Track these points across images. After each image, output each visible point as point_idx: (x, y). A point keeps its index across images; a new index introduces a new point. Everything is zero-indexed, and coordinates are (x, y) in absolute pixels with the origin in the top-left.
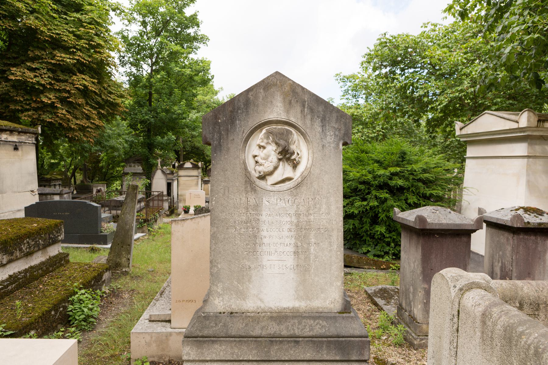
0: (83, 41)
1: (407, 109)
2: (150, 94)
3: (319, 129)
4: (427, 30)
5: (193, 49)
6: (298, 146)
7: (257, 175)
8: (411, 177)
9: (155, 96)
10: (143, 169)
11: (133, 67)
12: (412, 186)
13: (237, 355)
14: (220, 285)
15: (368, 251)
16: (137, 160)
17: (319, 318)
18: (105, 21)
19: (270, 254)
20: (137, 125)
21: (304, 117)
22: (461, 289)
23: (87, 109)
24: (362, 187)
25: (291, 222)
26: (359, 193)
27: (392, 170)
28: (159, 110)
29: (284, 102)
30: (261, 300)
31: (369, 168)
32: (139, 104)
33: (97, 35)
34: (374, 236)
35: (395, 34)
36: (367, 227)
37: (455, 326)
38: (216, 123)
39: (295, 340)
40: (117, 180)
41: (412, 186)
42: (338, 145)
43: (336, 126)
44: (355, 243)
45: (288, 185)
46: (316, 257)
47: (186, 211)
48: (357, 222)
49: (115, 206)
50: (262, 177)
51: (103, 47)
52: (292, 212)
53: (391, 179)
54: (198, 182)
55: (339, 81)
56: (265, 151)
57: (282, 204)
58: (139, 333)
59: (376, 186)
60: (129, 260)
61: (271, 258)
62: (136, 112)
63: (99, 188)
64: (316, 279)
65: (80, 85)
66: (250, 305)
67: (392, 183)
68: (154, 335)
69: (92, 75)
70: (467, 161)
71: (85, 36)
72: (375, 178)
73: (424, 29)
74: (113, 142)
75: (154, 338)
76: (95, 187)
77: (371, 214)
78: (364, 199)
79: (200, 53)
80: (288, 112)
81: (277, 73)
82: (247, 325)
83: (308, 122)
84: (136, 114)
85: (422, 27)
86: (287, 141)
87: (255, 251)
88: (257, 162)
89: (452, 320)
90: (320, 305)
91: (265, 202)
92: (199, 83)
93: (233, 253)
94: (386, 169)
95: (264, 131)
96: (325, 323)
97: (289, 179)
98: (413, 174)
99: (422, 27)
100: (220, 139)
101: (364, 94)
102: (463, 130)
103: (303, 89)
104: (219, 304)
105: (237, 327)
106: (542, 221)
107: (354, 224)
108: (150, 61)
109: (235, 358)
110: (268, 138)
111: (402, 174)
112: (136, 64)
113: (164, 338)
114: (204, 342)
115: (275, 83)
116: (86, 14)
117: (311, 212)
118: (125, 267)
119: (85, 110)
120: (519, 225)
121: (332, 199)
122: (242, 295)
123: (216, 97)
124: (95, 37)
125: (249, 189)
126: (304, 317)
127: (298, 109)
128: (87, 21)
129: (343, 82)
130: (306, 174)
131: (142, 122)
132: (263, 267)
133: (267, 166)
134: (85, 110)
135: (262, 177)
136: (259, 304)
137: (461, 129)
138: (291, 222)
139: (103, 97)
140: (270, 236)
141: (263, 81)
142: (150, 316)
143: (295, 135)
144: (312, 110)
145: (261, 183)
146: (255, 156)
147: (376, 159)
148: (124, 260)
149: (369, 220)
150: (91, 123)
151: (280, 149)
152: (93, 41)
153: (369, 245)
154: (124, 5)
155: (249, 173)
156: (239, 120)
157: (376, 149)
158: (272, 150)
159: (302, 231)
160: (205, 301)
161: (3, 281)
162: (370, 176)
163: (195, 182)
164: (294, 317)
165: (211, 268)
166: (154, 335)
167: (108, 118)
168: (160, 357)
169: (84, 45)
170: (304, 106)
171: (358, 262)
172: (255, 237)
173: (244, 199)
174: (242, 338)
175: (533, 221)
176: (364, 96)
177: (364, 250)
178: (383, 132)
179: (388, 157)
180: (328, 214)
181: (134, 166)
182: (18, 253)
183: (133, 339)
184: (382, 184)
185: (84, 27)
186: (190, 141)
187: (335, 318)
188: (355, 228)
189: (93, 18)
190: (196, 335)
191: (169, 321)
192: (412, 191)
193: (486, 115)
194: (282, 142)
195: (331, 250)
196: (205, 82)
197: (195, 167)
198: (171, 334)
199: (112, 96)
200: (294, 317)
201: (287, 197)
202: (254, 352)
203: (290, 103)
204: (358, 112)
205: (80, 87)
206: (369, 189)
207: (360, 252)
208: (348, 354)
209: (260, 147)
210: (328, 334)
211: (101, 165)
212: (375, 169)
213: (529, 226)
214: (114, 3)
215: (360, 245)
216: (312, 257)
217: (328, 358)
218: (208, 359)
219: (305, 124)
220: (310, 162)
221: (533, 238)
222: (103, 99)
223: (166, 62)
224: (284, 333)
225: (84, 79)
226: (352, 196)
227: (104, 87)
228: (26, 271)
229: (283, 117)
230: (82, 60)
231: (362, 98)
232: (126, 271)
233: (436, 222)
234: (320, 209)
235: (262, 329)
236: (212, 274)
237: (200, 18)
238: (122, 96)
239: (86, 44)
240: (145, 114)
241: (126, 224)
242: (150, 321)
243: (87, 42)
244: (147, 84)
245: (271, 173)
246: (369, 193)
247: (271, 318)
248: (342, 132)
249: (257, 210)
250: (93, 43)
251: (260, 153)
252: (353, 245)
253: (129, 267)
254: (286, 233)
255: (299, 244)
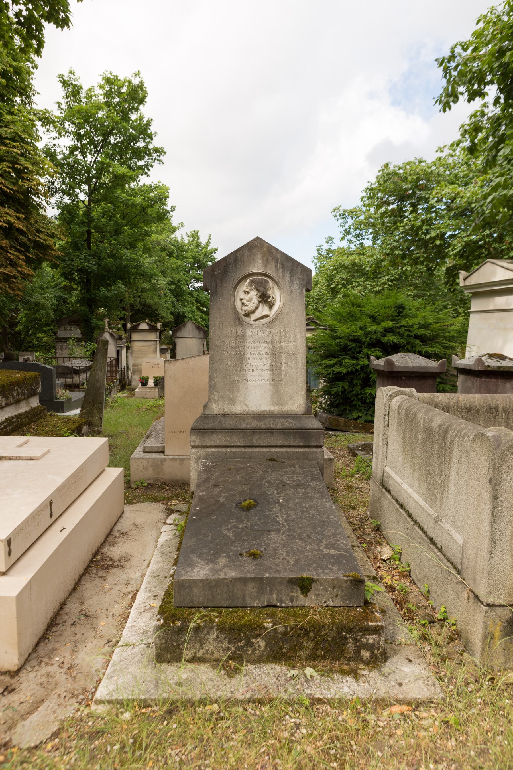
0: (5, 163)
1: (418, 255)
2: (89, 233)
3: (288, 279)
4: (443, 155)
5: (144, 170)
6: (273, 292)
7: (243, 313)
8: (407, 333)
9: (96, 235)
10: (82, 333)
11: (65, 197)
12: (408, 343)
13: (229, 442)
14: (216, 395)
15: (359, 417)
16: (73, 321)
17: (288, 417)
18: (30, 135)
19: (253, 371)
20: (74, 274)
21: (277, 270)
22: (391, 396)
23: (13, 254)
24: (353, 345)
25: (268, 348)
26: (349, 353)
27: (384, 324)
28: (104, 255)
29: (263, 259)
30: (246, 405)
31: (361, 324)
32: (75, 246)
33: (22, 155)
34: (365, 400)
35: (400, 163)
36: (357, 389)
37: (386, 424)
38: (213, 275)
39: (270, 431)
40: (37, 351)
41: (408, 343)
42: (302, 291)
43: (301, 277)
44: (345, 409)
45: (266, 320)
46: (286, 373)
47: (144, 383)
48: (346, 385)
49: (64, 374)
50: (247, 315)
51: (31, 172)
52: (269, 340)
53: (384, 336)
54: (156, 348)
55: (338, 217)
56: (249, 295)
57: (261, 334)
58: (138, 459)
59: (368, 344)
60: (101, 419)
61: (253, 374)
62: (72, 257)
63: (26, 357)
64: (287, 389)
65: (4, 222)
66: (238, 409)
67: (385, 340)
68: (150, 460)
69: (17, 209)
70: (472, 316)
71: (7, 156)
72: (367, 334)
73: (439, 154)
74: (38, 298)
75: (150, 464)
76: (21, 356)
77: (362, 375)
78: (354, 358)
79: (154, 176)
80: (265, 266)
81: (258, 238)
82: (236, 422)
83: (280, 274)
84: (72, 260)
85: (437, 151)
86: (265, 288)
87: (242, 369)
88: (243, 304)
89: (384, 418)
90: (289, 409)
91: (249, 333)
92: (154, 218)
93: (225, 370)
94: (379, 324)
95: (248, 281)
96: (292, 421)
97: (266, 316)
98: (408, 330)
99: (437, 151)
100: (216, 287)
101: (371, 233)
102: (467, 280)
103: (277, 249)
104: (216, 408)
105: (229, 423)
106: (502, 365)
107: (343, 387)
108: (86, 187)
109: (228, 444)
110: (251, 286)
111: (397, 330)
112: (69, 192)
113: (159, 463)
114: (206, 432)
115: (256, 246)
116: (6, 126)
117: (283, 340)
118: (97, 426)
119: (10, 255)
120: (480, 368)
121: (298, 331)
122: (232, 401)
123: (173, 236)
124: (20, 158)
125: (237, 323)
126: (277, 417)
127: (273, 264)
128: (9, 136)
129: (343, 218)
130: (279, 312)
131: (80, 271)
132: (247, 380)
133: (251, 306)
134: (10, 255)
135: (247, 315)
136: (245, 408)
137: (465, 279)
138: (268, 348)
139: (30, 237)
140: (253, 358)
141: (248, 244)
142: (145, 448)
143: (271, 284)
144: (283, 266)
145: (247, 319)
146: (241, 299)
147: (369, 313)
148: (96, 419)
149: (360, 381)
150: (18, 271)
151: (259, 294)
152: (19, 164)
153: (361, 411)
154: (54, 114)
155: (237, 311)
156: (230, 272)
157: (370, 303)
158: (254, 294)
159: (275, 355)
160: (205, 406)
161: (2, 422)
162: (360, 332)
163: (152, 348)
164: (270, 417)
165: (209, 382)
166: (150, 460)
167: (35, 264)
168: (157, 480)
169: (7, 170)
170: (277, 262)
171: (345, 425)
172: (242, 358)
173: (234, 330)
174: (233, 430)
175: (494, 365)
176: (371, 237)
177: (355, 415)
178: (389, 285)
179: (382, 311)
180: (295, 341)
181: (70, 329)
182: (11, 399)
183: (132, 462)
184: (374, 341)
185: (6, 145)
186: (139, 297)
187: (300, 417)
188: (344, 392)
189: (17, 133)
190: (199, 428)
191: (163, 452)
192: (407, 349)
193: (488, 264)
194: (261, 289)
195: (297, 368)
196: (162, 217)
197: (153, 329)
198: (165, 460)
199: (41, 235)
200: (270, 417)
201: (265, 329)
202: (241, 440)
203: (267, 260)
204: (360, 259)
205: (5, 225)
206: (360, 347)
207: (349, 418)
208: (309, 442)
209: (245, 292)
210: (294, 427)
211: (18, 329)
212: (368, 324)
213: (489, 369)
214: (41, 111)
215: (350, 411)
216: (283, 373)
217: (294, 444)
218: (208, 445)
219: (278, 275)
220: (282, 303)
221: (494, 380)
222: (29, 240)
223: (108, 189)
224: (263, 426)
225: (6, 213)
226: (341, 356)
227: (31, 224)
228: (16, 417)
229: (262, 271)
230: (6, 189)
231: (368, 239)
232: (98, 431)
233: (404, 365)
234: (289, 338)
235: (247, 424)
236: (210, 386)
237: (152, 129)
238: (52, 236)
239: (9, 167)
240: (82, 260)
241: (97, 381)
242: (144, 452)
243: (11, 165)
244: (85, 220)
245: (253, 312)
246: (360, 352)
247: (254, 417)
248: (305, 281)
249: (243, 339)
250: (19, 167)
251: (246, 297)
252: (343, 411)
253: (101, 426)
254: (264, 356)
255: (274, 364)
